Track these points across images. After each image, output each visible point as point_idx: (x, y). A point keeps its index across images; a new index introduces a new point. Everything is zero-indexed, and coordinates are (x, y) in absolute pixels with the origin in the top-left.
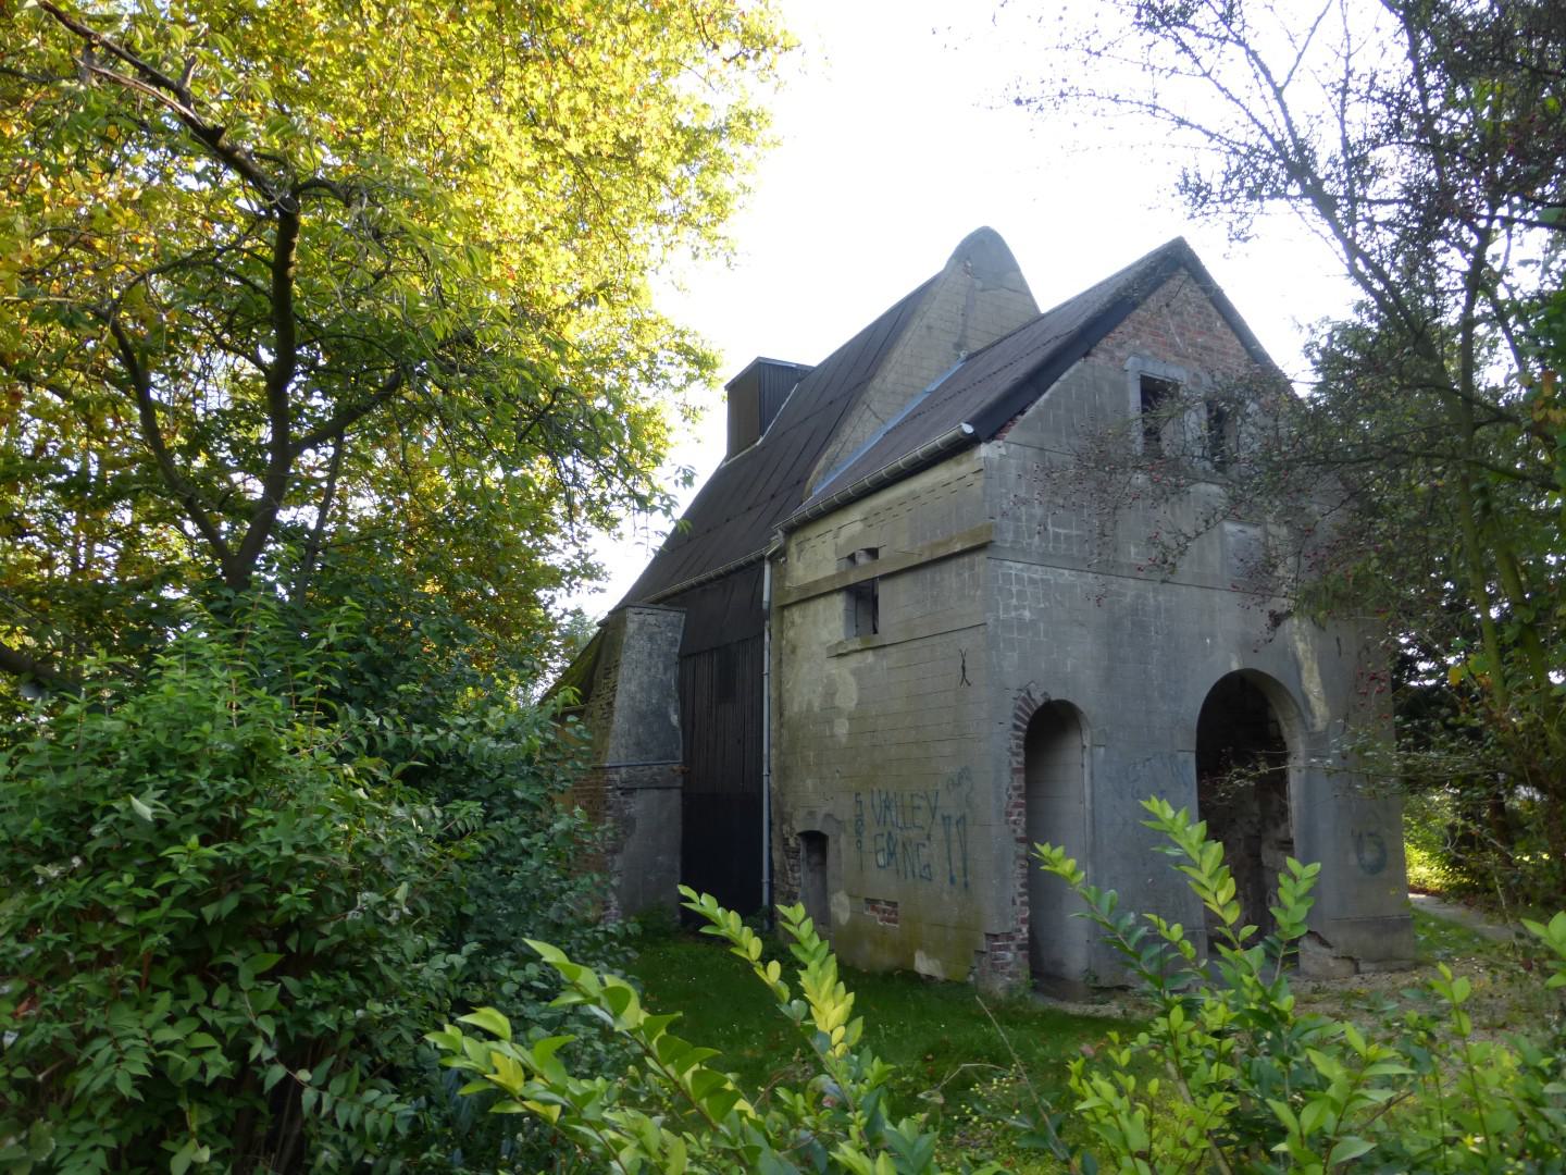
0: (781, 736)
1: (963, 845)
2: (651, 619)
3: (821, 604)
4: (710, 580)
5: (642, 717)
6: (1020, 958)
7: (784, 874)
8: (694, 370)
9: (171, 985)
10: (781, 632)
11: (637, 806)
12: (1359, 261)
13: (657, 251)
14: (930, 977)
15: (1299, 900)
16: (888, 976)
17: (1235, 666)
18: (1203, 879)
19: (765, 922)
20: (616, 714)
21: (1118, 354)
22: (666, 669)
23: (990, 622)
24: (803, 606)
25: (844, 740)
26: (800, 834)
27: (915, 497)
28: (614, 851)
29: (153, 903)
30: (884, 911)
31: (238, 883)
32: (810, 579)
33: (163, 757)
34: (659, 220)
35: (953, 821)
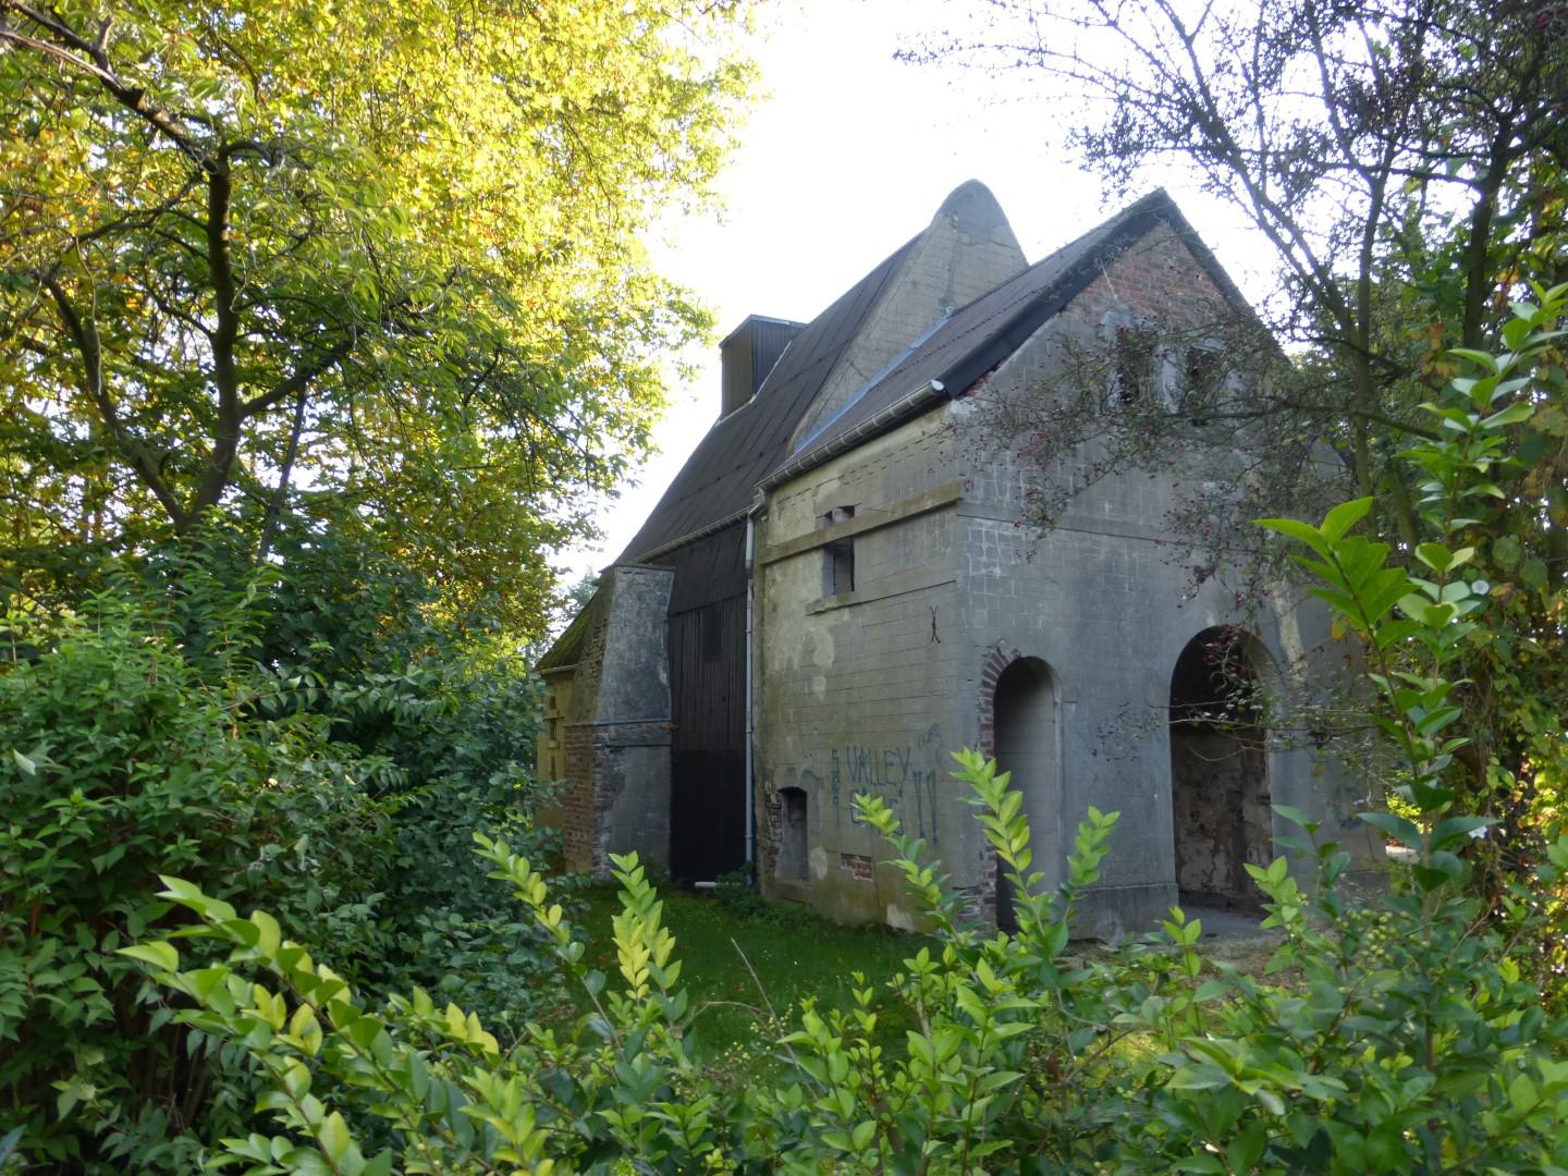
0: (763, 692)
1: (933, 800)
2: (640, 579)
3: (801, 561)
4: (698, 539)
5: (631, 675)
6: (987, 911)
7: (767, 831)
8: (690, 328)
9: (61, 932)
10: (763, 590)
11: (626, 764)
12: (1267, 213)
13: (648, 209)
14: (902, 930)
15: (1094, 849)
16: (861, 929)
17: (1211, 622)
18: (999, 827)
19: (749, 878)
20: (605, 673)
21: (1095, 309)
22: (655, 628)
23: (960, 579)
24: (783, 564)
25: (822, 697)
26: (781, 791)
27: (889, 454)
28: (604, 808)
29: (36, 854)
30: (859, 866)
31: (128, 835)
32: (790, 537)
33: (60, 714)
34: (648, 175)
35: (924, 776)
